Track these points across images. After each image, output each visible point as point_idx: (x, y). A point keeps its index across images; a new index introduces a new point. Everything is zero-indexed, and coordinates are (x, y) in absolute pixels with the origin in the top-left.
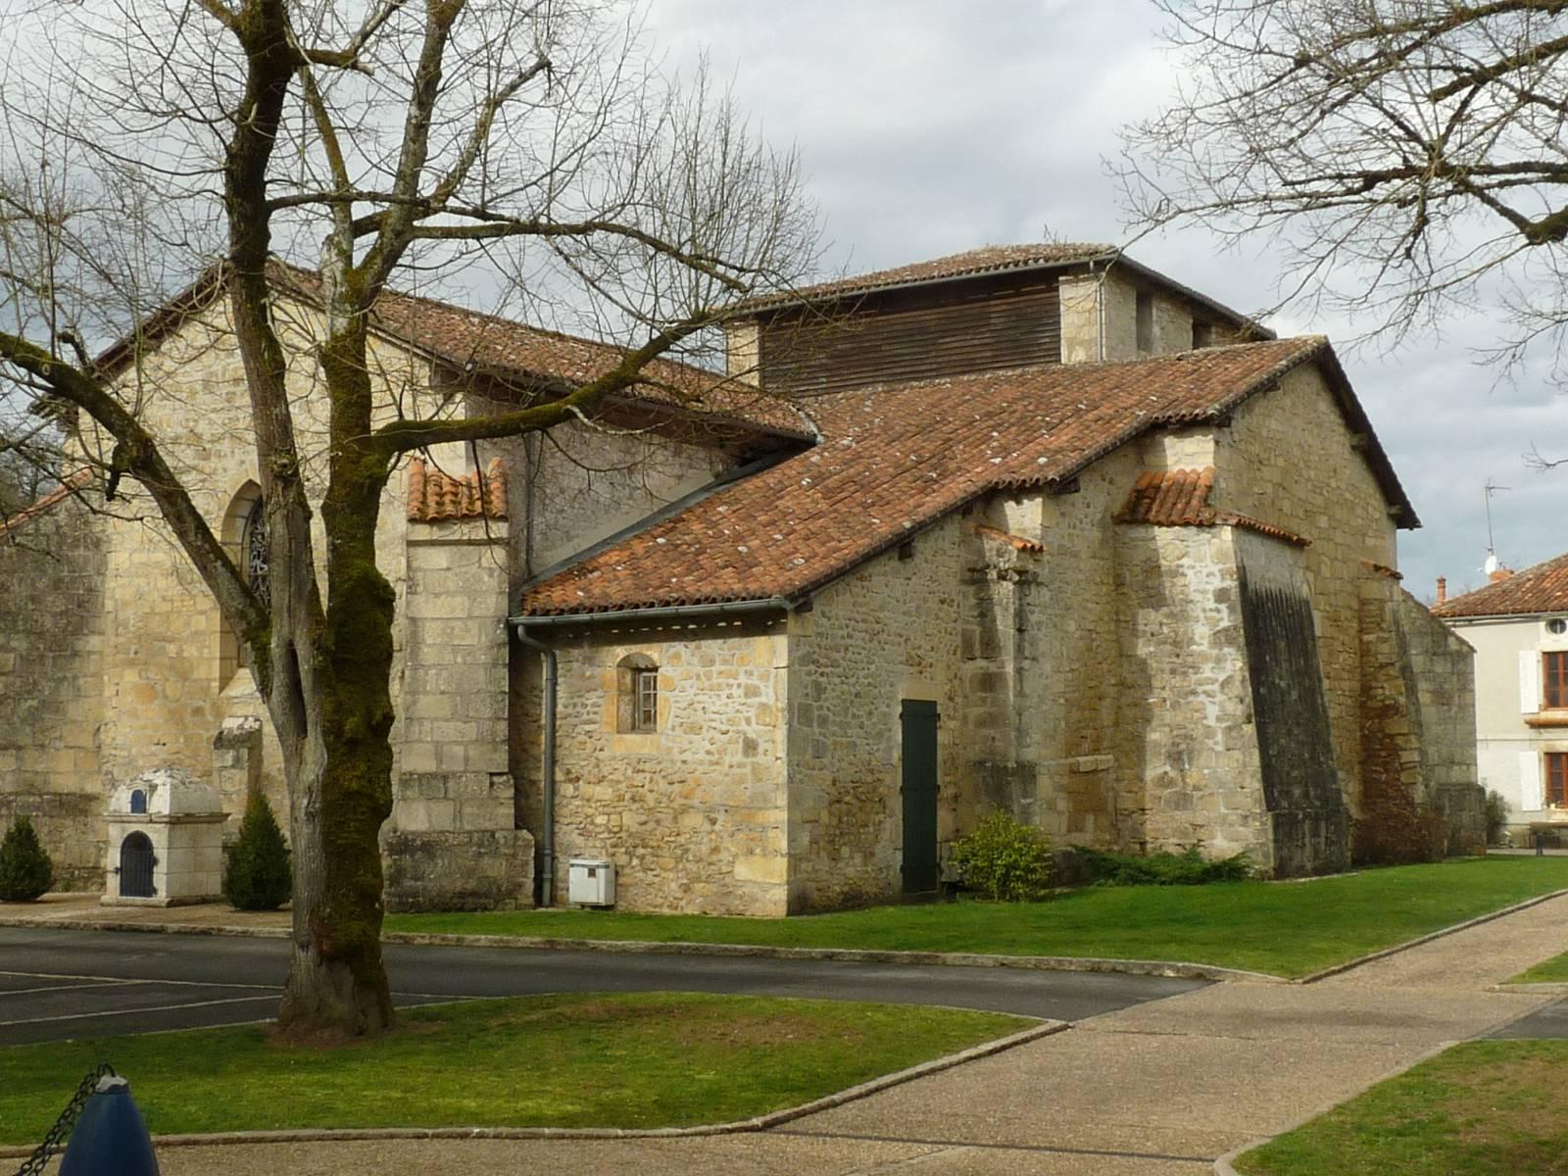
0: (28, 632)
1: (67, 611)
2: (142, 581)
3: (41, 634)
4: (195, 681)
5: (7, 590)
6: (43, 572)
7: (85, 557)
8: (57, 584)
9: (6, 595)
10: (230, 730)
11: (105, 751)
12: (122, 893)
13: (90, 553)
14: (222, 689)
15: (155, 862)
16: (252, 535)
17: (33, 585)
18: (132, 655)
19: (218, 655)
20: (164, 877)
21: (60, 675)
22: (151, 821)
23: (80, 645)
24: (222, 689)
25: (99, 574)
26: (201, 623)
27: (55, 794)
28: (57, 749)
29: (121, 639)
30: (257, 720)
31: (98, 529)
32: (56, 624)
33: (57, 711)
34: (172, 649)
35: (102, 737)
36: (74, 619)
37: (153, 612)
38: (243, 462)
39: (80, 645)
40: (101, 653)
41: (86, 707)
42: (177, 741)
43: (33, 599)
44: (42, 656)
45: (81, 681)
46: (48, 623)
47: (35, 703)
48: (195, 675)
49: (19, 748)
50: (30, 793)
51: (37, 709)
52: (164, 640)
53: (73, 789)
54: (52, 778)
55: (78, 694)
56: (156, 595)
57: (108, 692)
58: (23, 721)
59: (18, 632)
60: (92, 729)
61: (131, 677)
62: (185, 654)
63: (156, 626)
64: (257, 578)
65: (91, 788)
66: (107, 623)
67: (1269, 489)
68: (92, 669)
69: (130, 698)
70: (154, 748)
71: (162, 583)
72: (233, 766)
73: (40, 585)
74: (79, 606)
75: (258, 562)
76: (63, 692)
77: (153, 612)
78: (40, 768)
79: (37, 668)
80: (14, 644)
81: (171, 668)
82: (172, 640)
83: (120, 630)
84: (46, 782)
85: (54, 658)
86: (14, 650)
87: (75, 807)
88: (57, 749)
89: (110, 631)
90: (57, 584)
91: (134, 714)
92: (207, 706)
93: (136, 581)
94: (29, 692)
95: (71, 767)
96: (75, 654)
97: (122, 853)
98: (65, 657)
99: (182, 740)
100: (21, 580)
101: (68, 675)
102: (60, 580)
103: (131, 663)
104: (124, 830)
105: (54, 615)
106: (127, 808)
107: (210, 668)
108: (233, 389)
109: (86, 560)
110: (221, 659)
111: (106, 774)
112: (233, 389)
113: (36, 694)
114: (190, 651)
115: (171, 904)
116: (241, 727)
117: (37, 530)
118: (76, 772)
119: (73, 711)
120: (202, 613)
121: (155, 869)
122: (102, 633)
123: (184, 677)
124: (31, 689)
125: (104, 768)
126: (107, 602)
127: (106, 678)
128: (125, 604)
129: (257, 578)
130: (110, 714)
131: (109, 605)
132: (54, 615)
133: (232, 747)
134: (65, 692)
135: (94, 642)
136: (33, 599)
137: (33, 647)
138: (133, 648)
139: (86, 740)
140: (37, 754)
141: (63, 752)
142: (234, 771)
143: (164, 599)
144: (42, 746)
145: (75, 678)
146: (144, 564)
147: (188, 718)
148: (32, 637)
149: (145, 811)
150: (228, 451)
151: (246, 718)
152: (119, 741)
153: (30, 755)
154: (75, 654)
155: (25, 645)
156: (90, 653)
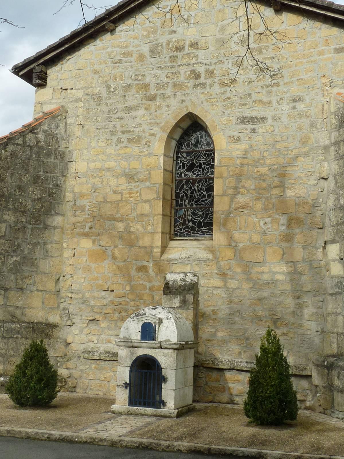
0: (16, 210)
1: (42, 198)
2: (96, 181)
3: (24, 212)
4: (141, 247)
5: (2, 180)
6: (27, 171)
7: (54, 164)
8: (36, 179)
9: (2, 184)
10: (174, 282)
11: (63, 294)
12: (131, 403)
13: (58, 162)
14: (162, 253)
15: (164, 379)
16: (178, 153)
17: (20, 179)
18: (87, 229)
19: (160, 230)
20: (173, 393)
21: (35, 241)
22: (161, 347)
23: (49, 221)
24: (162, 253)
25: (63, 176)
26: (146, 208)
27: (29, 323)
28: (31, 292)
29: (80, 219)
30: (195, 275)
31: (64, 146)
32: (34, 207)
33: (33, 265)
34: (121, 226)
35: (61, 284)
36: (46, 204)
37: (105, 201)
38: (183, 101)
39: (49, 221)
40: (62, 228)
41: (52, 263)
42: (123, 288)
43: (20, 188)
44: (24, 227)
45: (49, 246)
46: (29, 205)
47: (18, 259)
48: (141, 243)
49: (6, 290)
50: (13, 322)
51: (19, 263)
52: (115, 220)
53: (41, 320)
54: (27, 311)
55: (47, 255)
56: (108, 190)
57: (67, 254)
58: (10, 271)
59: (9, 210)
60: (55, 278)
61: (86, 244)
62: (132, 229)
63: (107, 210)
64: (181, 181)
65: (54, 318)
66: (67, 208)
67: (16, 243)
68: (56, 238)
69: (85, 259)
70: (103, 293)
71: (113, 182)
72: (180, 307)
73: (25, 179)
74: (49, 196)
75: (183, 171)
76: (37, 253)
77: (105, 201)
78: (19, 304)
79: (21, 236)
80: (6, 217)
81: (121, 238)
82: (121, 220)
83: (78, 213)
84: (23, 314)
85: (32, 229)
86: (5, 221)
87: (43, 332)
88: (31, 292)
89: (69, 213)
90: (36, 179)
91: (88, 269)
92: (151, 265)
93: (92, 181)
94: (15, 251)
95: (40, 305)
96: (46, 227)
97: (131, 371)
98: (38, 229)
99: (128, 288)
100: (12, 174)
101: (41, 241)
102: (38, 177)
103: (86, 235)
104: (133, 354)
105: (33, 200)
106: (136, 336)
107: (153, 239)
108: (175, 54)
109: (55, 166)
110: (162, 233)
111: (64, 310)
112: (175, 54)
113: (19, 252)
114: (137, 227)
115: (179, 415)
116: (183, 280)
117: (24, 142)
118: (43, 309)
119: (44, 265)
120: (146, 201)
121: (164, 386)
122: (63, 215)
123: (131, 245)
124: (16, 249)
125: (62, 306)
126: (67, 194)
127: (65, 245)
128: (82, 196)
129: (181, 181)
130: (68, 269)
131: (69, 196)
132: (33, 200)
133: (179, 293)
134: (38, 253)
135: (58, 220)
136: (20, 188)
137: (18, 221)
138: (88, 225)
139: (50, 285)
140: (18, 294)
141: (35, 293)
142: (181, 311)
143: (115, 192)
144: (22, 289)
145: (45, 244)
146: (101, 170)
147: (133, 272)
148: (18, 214)
149: (154, 339)
150: (171, 94)
151: (186, 274)
152: (75, 287)
153: (12, 294)
154: (46, 227)
155: (13, 219)
156: (55, 228)
